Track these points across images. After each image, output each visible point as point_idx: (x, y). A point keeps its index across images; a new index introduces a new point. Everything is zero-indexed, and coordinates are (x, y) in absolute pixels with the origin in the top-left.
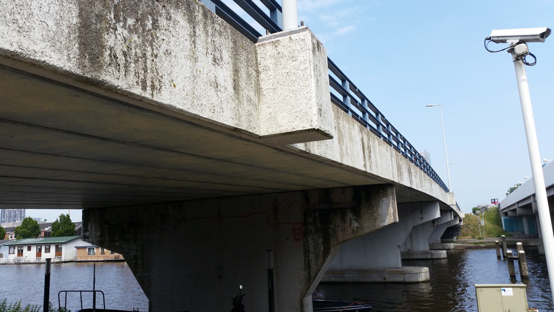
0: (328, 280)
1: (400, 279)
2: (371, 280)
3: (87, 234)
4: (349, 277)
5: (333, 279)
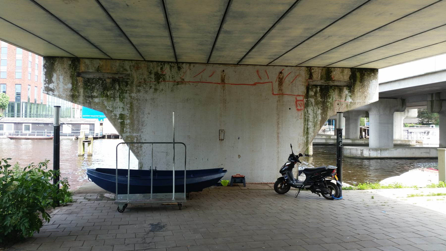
3: (51, 86)
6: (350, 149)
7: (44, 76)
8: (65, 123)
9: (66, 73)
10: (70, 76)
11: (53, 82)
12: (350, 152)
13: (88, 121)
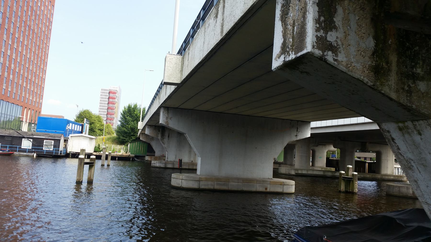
0: (212, 187)
1: (279, 190)
2: (254, 189)
3: (332, 37)
4: (233, 186)
5: (217, 187)
6: (399, 187)
7: (317, 8)
8: (25, 136)
9: (362, 9)
10: (372, 19)
11: (335, 28)
12: (399, 191)
13: (52, 136)
